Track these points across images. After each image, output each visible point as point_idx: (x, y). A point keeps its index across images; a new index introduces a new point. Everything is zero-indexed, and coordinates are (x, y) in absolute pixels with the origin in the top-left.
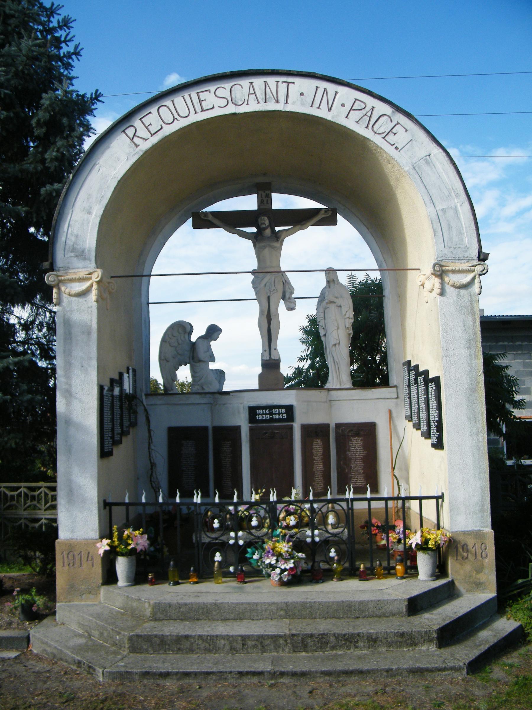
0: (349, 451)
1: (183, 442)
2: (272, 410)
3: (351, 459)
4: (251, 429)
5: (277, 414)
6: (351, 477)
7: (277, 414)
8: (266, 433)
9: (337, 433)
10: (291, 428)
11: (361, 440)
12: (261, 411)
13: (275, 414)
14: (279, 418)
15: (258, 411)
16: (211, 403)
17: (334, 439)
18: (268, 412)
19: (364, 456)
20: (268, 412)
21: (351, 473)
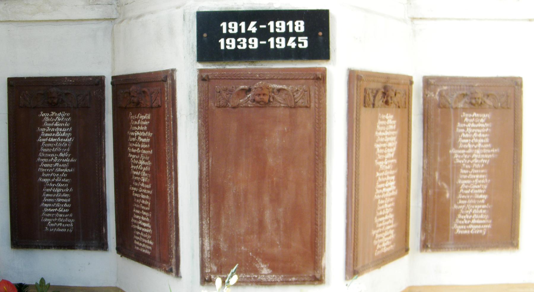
0: (456, 146)
1: (42, 114)
2: (266, 23)
3: (459, 167)
4: (204, 79)
5: (281, 35)
6: (457, 212)
7: (281, 35)
8: (249, 90)
9: (426, 101)
10: (320, 79)
11: (487, 121)
12: (234, 27)
13: (276, 35)
14: (288, 48)
15: (224, 25)
16: (112, 20)
17: (421, 117)
18: (254, 30)
19: (492, 160)
20: (254, 30)
21: (456, 201)
